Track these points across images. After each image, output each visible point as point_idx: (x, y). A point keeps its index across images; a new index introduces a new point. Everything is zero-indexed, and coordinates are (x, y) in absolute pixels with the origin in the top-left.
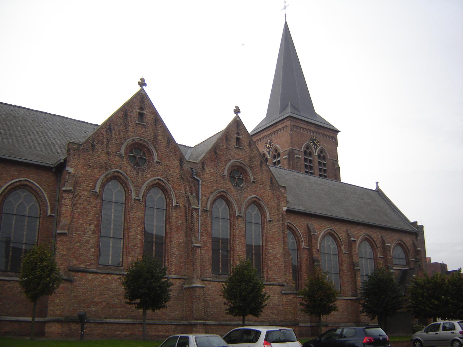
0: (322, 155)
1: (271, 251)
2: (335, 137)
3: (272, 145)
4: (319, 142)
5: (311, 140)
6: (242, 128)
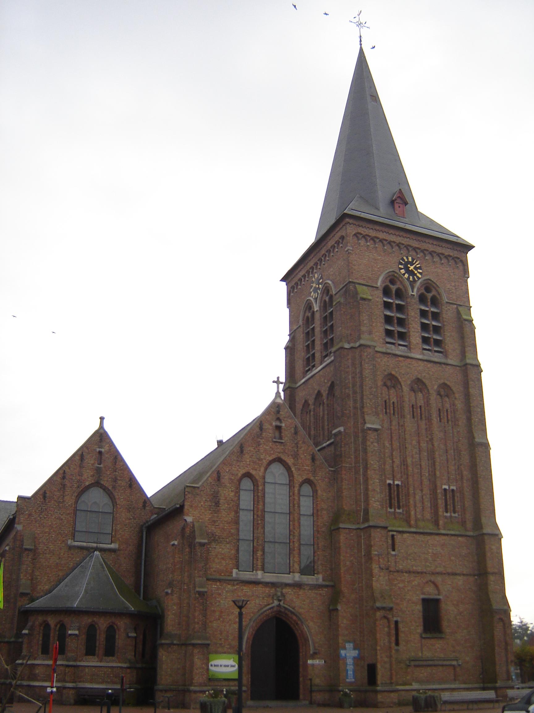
0: (429, 296)
1: (348, 563)
2: (463, 259)
4: (420, 268)
5: (401, 264)
6: (121, 464)
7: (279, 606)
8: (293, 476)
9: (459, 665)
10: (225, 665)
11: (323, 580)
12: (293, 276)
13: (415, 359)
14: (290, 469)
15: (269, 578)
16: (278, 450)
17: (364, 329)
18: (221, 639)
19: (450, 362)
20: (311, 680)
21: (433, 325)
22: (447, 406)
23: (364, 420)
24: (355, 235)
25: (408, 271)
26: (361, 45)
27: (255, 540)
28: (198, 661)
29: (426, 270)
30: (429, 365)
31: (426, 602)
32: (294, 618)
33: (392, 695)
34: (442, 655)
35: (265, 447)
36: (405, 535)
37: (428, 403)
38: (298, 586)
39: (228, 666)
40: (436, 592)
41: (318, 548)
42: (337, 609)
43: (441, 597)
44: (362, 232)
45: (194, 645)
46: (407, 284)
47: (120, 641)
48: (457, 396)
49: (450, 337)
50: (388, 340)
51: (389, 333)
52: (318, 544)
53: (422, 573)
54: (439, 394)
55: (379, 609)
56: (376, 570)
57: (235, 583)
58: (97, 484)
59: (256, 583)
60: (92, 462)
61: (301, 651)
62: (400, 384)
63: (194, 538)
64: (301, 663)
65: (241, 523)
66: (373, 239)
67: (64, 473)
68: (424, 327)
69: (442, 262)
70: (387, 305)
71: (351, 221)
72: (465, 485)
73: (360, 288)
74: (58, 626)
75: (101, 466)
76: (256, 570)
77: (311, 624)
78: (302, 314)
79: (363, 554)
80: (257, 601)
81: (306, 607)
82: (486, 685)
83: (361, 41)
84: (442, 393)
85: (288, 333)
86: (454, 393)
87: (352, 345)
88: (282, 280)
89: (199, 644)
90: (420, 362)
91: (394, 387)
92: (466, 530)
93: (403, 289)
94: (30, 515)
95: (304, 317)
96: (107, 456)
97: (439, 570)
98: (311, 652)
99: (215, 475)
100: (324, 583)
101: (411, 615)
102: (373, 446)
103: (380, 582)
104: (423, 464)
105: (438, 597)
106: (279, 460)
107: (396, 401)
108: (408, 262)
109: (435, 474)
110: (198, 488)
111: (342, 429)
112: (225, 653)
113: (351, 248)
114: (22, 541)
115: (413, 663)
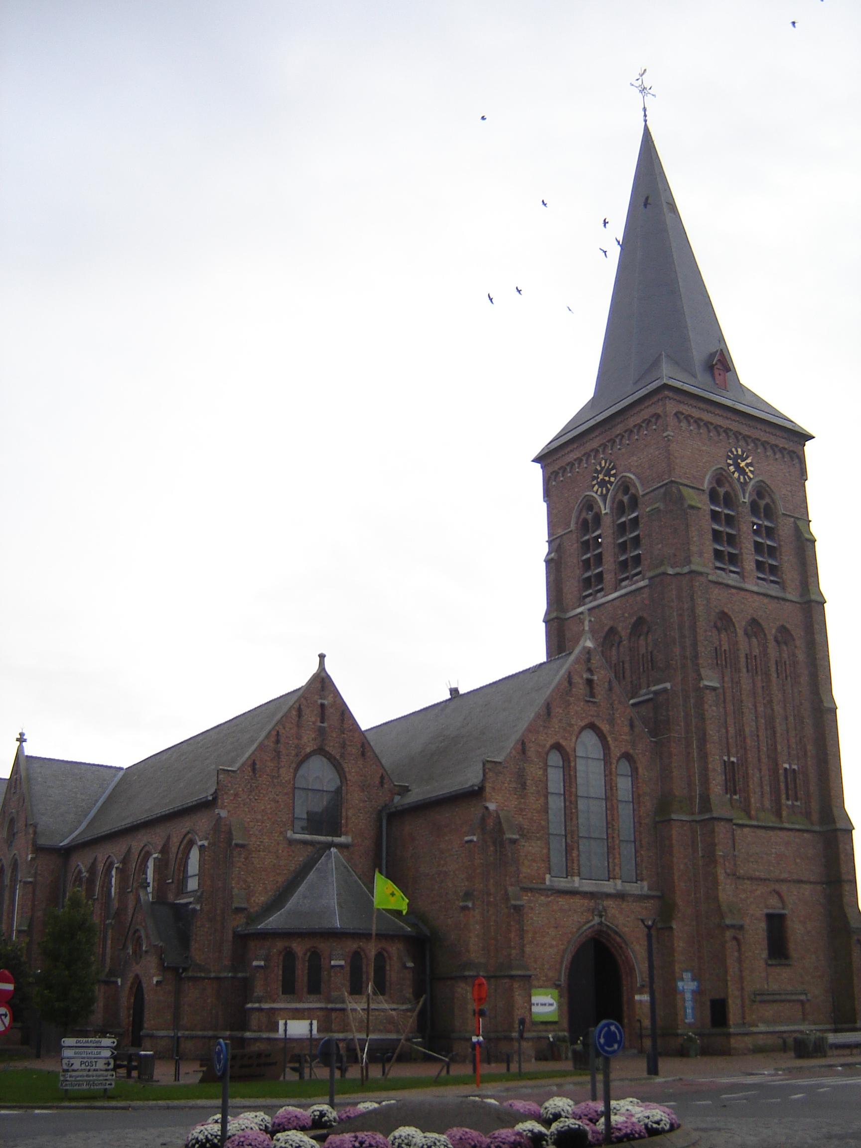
0: (762, 503)
3: (614, 475)
5: (729, 457)
6: (350, 722)
7: (601, 923)
8: (609, 749)
9: (808, 1000)
10: (545, 1004)
11: (649, 889)
12: (557, 457)
13: (748, 593)
14: (605, 738)
15: (588, 886)
16: (591, 713)
17: (694, 549)
18: (535, 969)
19: (789, 596)
20: (639, 1021)
21: (768, 545)
22: (785, 655)
23: (700, 675)
24: (676, 414)
25: (737, 466)
26: (646, 121)
27: (569, 836)
28: (519, 999)
29: (754, 469)
30: (766, 600)
31: (770, 917)
32: (618, 939)
33: (746, 1038)
34: (789, 988)
35: (575, 708)
36: (746, 830)
37: (765, 652)
38: (621, 896)
39: (545, 1005)
40: (780, 905)
41: (642, 847)
42: (671, 928)
44: (684, 411)
45: (512, 977)
46: (738, 487)
47: (393, 973)
48: (798, 643)
49: (787, 561)
50: (718, 564)
51: (718, 555)
52: (641, 841)
53: (765, 880)
54: (777, 641)
55: (729, 927)
56: (722, 877)
57: (549, 893)
58: (320, 751)
59: (573, 893)
60: (313, 719)
61: (624, 982)
62: (734, 626)
63: (501, 831)
64: (625, 999)
65: (550, 812)
66: (697, 421)
67: (278, 734)
68: (758, 547)
69: (777, 457)
70: (715, 516)
71: (671, 394)
72: (809, 763)
73: (686, 491)
74: (309, 954)
75: (325, 725)
76: (572, 876)
77: (637, 947)
78: (574, 514)
79: (700, 855)
80: (575, 918)
81: (629, 923)
82: (839, 1026)
83: (645, 116)
84: (780, 639)
86: (794, 640)
87: (678, 570)
89: (520, 976)
90: (755, 596)
91: (726, 630)
92: (812, 824)
93: (733, 495)
94: (236, 795)
95: (578, 518)
96: (331, 710)
97: (784, 876)
98: (638, 985)
99: (519, 746)
100: (650, 893)
101: (757, 933)
102: (712, 711)
103: (726, 892)
104: (760, 734)
105: (783, 912)
106: (592, 726)
107: (727, 649)
108: (737, 457)
109: (776, 749)
110: (500, 763)
111: (668, 685)
112: (541, 987)
113: (672, 434)
114: (230, 833)
115: (758, 998)
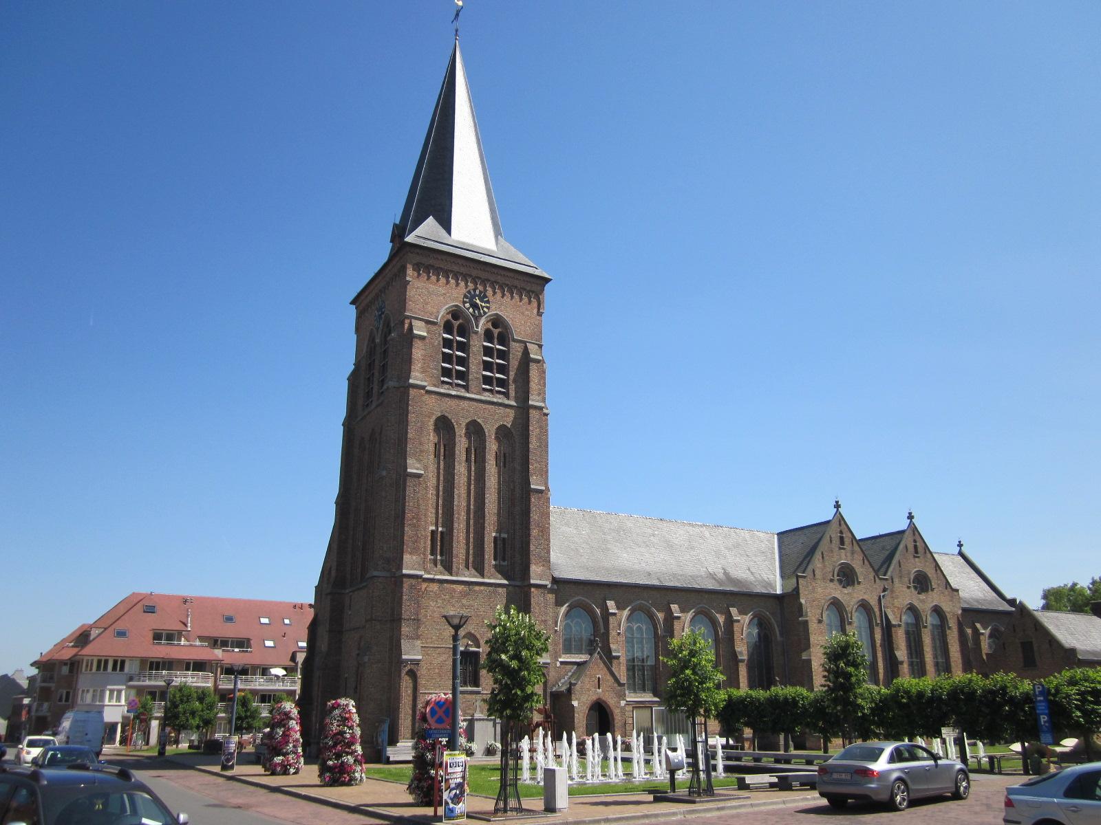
43: (481, 650)
85: (354, 362)
88: (353, 303)
